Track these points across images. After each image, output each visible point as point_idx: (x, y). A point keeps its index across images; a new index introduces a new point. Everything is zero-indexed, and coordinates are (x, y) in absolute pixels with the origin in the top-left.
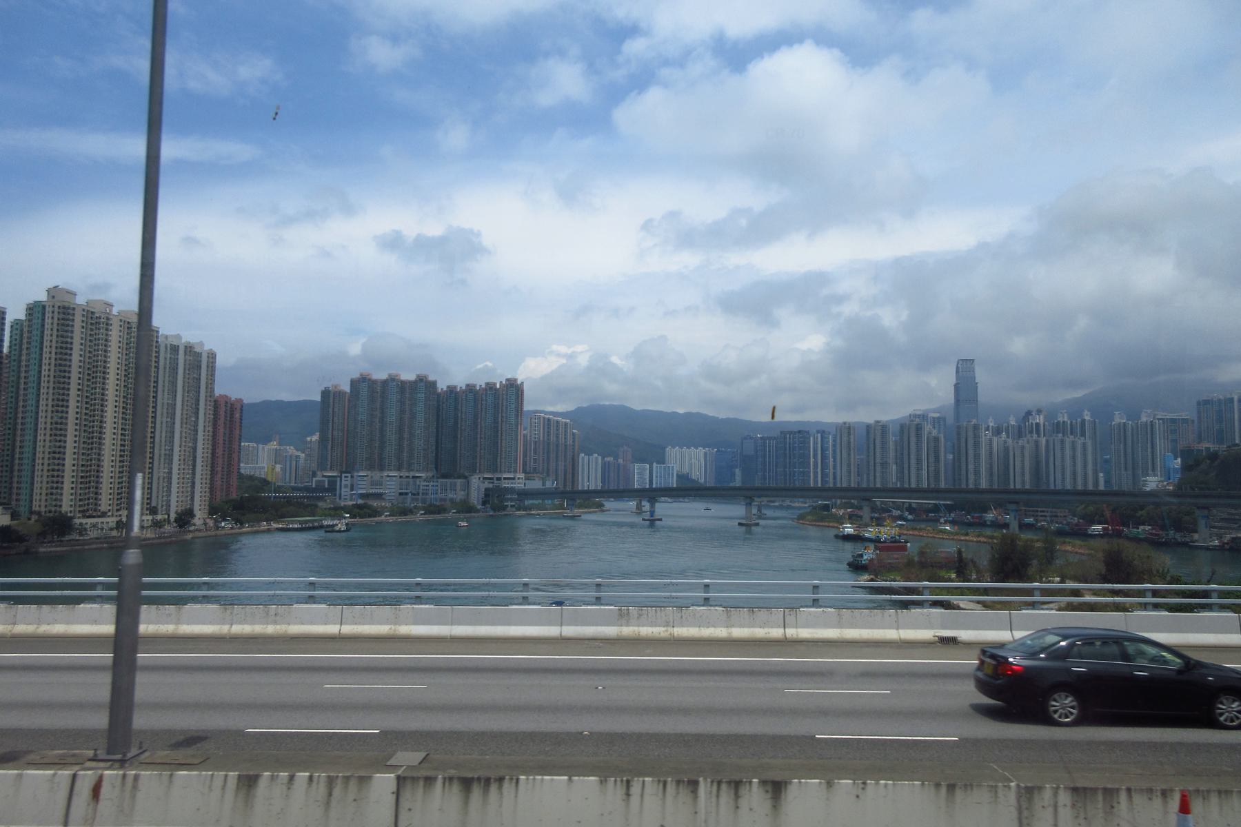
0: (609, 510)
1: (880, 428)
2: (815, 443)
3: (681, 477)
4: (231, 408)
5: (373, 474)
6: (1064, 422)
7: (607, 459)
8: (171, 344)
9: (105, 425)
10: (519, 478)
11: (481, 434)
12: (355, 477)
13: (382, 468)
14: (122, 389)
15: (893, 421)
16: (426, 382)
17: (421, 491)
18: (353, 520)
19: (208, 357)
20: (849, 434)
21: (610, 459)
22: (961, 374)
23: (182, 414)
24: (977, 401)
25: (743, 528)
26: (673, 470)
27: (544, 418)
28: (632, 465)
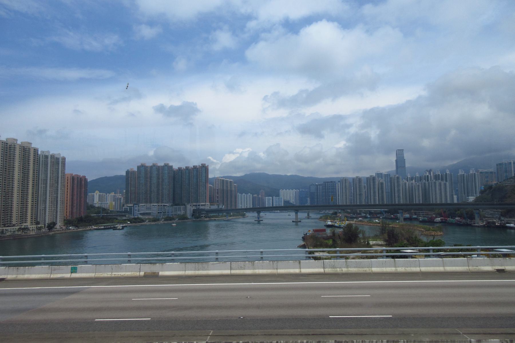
0: (248, 217)
2: (338, 186)
3: (285, 202)
4: (80, 180)
6: (438, 175)
8: (45, 155)
9: (14, 189)
10: (207, 205)
13: (151, 203)
14: (21, 174)
16: (168, 166)
17: (167, 211)
18: (131, 224)
19: (62, 160)
20: (346, 182)
21: (256, 195)
23: (50, 183)
25: (294, 223)
26: (282, 199)
27: (221, 180)
28: (265, 197)
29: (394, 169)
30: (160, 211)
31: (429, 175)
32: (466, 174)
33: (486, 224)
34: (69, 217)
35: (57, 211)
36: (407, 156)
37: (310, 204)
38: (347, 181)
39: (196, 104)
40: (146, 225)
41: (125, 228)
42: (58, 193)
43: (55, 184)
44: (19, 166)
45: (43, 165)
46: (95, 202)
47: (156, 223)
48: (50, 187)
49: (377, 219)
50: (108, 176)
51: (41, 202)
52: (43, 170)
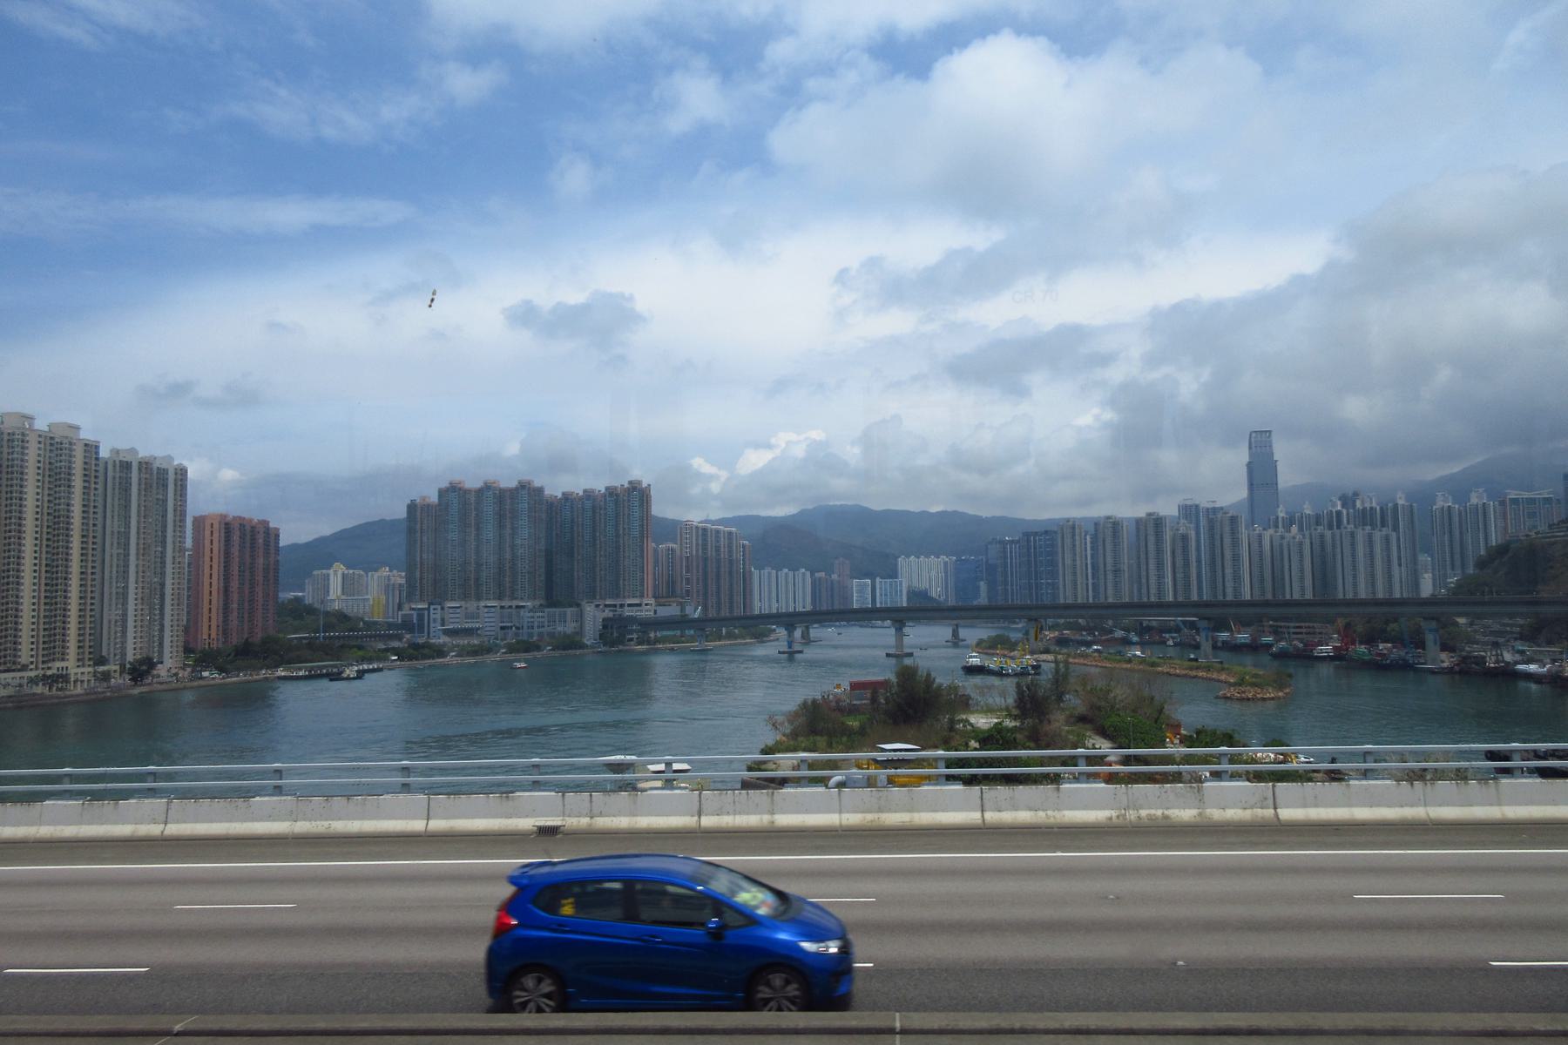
1: (1110, 525)
3: (914, 594)
5: (468, 605)
6: (1371, 508)
7: (817, 575)
8: (120, 461)
10: (646, 605)
11: (600, 551)
12: (446, 609)
13: (479, 598)
15: (1128, 519)
19: (176, 474)
20: (1074, 535)
21: (822, 574)
22: (1254, 449)
24: (1277, 484)
29: (1242, 493)
30: (504, 624)
31: (1345, 512)
32: (1457, 506)
33: (1458, 665)
34: (215, 642)
35: (162, 626)
36: (1282, 451)
37: (986, 600)
38: (1077, 531)
39: (631, 298)
40: (446, 666)
41: (366, 675)
42: (165, 572)
43: (156, 546)
44: (38, 494)
45: (117, 491)
46: (332, 596)
47: (479, 658)
48: (137, 554)
49: (1138, 647)
50: (388, 518)
51: (110, 599)
52: (116, 506)
